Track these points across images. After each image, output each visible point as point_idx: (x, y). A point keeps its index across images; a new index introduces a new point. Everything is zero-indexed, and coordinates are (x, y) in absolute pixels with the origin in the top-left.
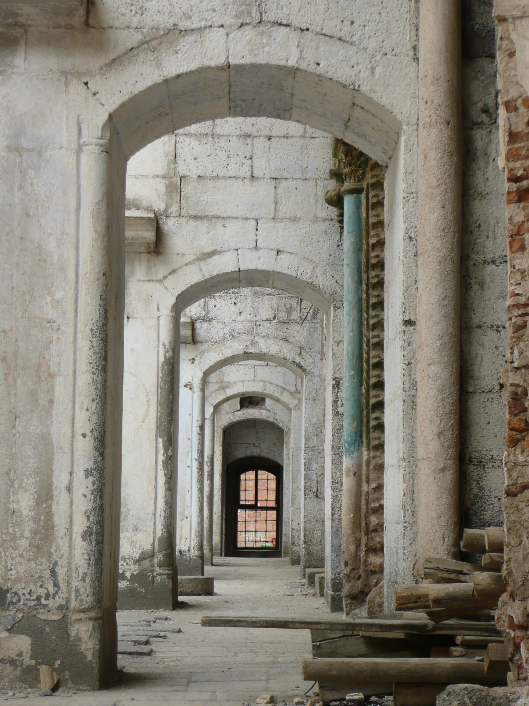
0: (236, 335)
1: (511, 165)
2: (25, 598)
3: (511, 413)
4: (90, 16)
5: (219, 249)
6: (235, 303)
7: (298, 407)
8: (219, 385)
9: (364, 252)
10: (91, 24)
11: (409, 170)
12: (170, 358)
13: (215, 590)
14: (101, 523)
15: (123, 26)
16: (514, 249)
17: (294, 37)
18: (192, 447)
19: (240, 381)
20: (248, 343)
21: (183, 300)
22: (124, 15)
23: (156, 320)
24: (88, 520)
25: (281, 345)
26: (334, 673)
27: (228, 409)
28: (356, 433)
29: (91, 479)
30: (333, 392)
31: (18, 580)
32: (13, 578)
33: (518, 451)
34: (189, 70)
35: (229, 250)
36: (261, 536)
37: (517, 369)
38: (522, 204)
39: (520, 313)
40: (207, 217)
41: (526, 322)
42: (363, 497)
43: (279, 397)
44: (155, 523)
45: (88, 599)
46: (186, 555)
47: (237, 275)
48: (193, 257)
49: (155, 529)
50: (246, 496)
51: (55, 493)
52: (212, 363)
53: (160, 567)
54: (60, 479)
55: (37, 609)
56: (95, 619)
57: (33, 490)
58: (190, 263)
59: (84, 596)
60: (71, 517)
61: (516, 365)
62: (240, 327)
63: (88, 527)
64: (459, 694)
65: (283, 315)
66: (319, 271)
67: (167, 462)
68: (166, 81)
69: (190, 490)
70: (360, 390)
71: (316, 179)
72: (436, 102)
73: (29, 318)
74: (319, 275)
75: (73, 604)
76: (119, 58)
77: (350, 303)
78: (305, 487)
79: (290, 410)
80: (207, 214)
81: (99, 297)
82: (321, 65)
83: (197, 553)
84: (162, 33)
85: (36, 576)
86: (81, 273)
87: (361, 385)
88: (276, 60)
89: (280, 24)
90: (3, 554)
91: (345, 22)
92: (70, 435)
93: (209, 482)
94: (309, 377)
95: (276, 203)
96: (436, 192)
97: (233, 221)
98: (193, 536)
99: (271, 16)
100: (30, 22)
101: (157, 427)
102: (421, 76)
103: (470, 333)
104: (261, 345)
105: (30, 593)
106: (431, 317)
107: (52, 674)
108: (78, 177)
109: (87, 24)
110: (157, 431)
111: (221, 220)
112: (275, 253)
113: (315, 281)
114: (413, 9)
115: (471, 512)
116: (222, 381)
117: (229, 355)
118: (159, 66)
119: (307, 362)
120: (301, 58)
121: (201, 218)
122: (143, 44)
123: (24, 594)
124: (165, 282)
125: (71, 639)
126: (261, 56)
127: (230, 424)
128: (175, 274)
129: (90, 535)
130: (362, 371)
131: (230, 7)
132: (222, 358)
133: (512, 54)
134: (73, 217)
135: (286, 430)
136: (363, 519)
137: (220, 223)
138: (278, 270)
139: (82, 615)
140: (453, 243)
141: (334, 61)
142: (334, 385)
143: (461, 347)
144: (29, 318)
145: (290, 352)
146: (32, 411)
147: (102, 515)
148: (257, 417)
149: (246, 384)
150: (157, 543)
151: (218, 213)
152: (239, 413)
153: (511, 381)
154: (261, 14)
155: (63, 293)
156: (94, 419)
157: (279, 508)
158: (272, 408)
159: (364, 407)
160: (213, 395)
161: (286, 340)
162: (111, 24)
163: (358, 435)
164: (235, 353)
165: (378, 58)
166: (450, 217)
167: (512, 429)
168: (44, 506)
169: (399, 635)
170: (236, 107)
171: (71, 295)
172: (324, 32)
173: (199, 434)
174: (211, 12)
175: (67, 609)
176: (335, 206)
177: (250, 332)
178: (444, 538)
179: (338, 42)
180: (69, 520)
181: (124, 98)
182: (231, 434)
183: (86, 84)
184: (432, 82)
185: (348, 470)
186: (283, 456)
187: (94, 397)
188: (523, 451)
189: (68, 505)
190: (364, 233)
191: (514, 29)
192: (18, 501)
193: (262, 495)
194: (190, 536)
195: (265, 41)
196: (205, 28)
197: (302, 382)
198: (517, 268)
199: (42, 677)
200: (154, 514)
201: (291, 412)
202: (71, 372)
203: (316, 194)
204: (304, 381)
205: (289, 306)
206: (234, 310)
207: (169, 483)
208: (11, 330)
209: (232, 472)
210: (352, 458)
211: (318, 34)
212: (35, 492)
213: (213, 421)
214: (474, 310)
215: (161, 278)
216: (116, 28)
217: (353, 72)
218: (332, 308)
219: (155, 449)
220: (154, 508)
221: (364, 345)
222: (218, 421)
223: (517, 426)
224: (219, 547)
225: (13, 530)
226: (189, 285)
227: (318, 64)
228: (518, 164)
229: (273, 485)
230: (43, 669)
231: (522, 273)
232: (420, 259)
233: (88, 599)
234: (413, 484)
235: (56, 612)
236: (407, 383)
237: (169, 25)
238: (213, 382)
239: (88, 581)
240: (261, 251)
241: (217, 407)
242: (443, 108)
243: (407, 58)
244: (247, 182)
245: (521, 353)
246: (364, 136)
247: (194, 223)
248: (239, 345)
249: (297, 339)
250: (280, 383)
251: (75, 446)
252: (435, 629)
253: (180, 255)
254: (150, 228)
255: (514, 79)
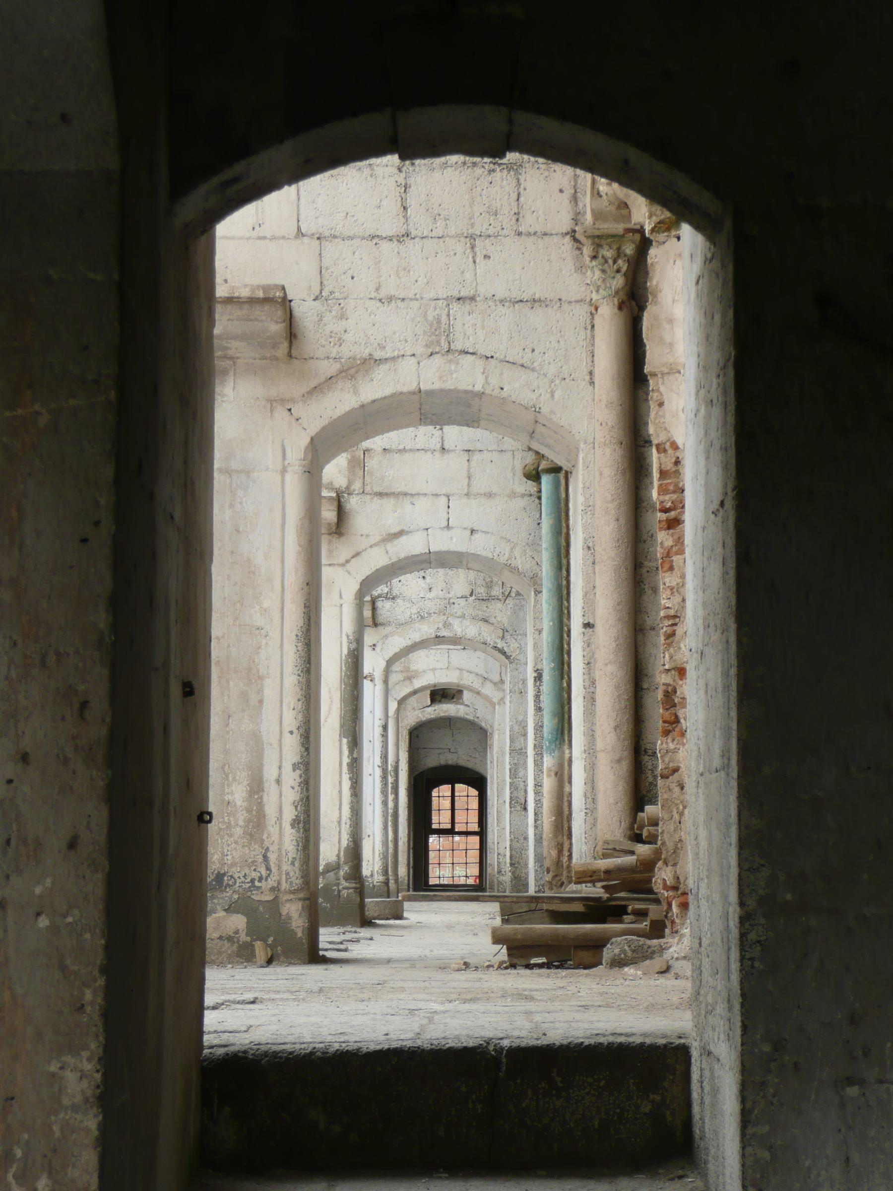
5: (407, 529)
6: (424, 577)
8: (405, 674)
9: (563, 535)
10: (293, 355)
11: (587, 485)
12: (354, 650)
13: (405, 915)
14: (307, 812)
16: (665, 569)
17: (480, 364)
18: (373, 751)
20: (440, 625)
21: (367, 584)
22: (323, 346)
26: (519, 937)
29: (298, 772)
30: (535, 685)
31: (234, 864)
32: (229, 862)
33: (669, 740)
35: (418, 530)
36: (459, 871)
37: (668, 670)
38: (671, 531)
40: (394, 493)
42: (566, 799)
44: (340, 832)
45: (297, 881)
47: (427, 557)
48: (378, 538)
50: (440, 818)
51: (266, 785)
52: (397, 650)
53: (346, 879)
54: (270, 773)
57: (245, 783)
58: (376, 545)
59: (293, 879)
61: (667, 667)
62: (430, 606)
66: (517, 553)
68: (363, 406)
70: (562, 684)
72: (610, 424)
73: (240, 625)
75: (284, 886)
77: (550, 590)
78: (511, 798)
79: (493, 705)
80: (393, 491)
85: (250, 860)
86: (286, 583)
87: (562, 678)
88: (462, 386)
89: (467, 353)
93: (393, 796)
96: (611, 506)
97: (422, 497)
98: (377, 859)
99: (458, 345)
101: (342, 726)
103: (644, 634)
104: (455, 627)
105: (245, 876)
108: (283, 496)
109: (290, 355)
112: (469, 532)
113: (513, 563)
114: (589, 337)
116: (407, 670)
118: (356, 392)
119: (511, 647)
120: (487, 382)
121: (387, 495)
123: (239, 877)
124: (348, 565)
125: (283, 917)
128: (359, 558)
129: (298, 824)
131: (421, 337)
132: (409, 643)
133: (661, 404)
134: (279, 533)
135: (490, 731)
136: (565, 822)
137: (407, 500)
138: (472, 552)
139: (292, 896)
140: (626, 553)
141: (517, 385)
143: (636, 647)
145: (491, 635)
146: (243, 711)
147: (308, 806)
149: (437, 673)
150: (342, 853)
152: (430, 709)
153: (663, 681)
155: (270, 602)
156: (300, 717)
157: (482, 833)
159: (566, 702)
160: (397, 687)
161: (485, 621)
164: (425, 637)
165: (557, 382)
167: (664, 722)
169: (578, 907)
170: (426, 419)
172: (507, 359)
173: (383, 736)
175: (279, 890)
177: (442, 612)
179: (520, 368)
181: (325, 422)
182: (418, 736)
183: (290, 410)
184: (606, 406)
185: (549, 770)
187: (299, 697)
188: (673, 740)
189: (278, 796)
190: (563, 514)
191: (663, 383)
192: (232, 793)
193: (460, 817)
195: (453, 368)
196: (398, 357)
199: (257, 951)
200: (339, 822)
201: (494, 708)
203: (513, 469)
206: (423, 585)
208: (223, 637)
209: (422, 785)
211: (501, 361)
212: (248, 785)
213: (397, 720)
215: (344, 562)
218: (533, 593)
219: (338, 750)
221: (565, 635)
224: (406, 882)
226: (374, 569)
227: (502, 389)
228: (667, 497)
229: (474, 804)
230: (258, 944)
232: (597, 567)
233: (297, 881)
236: (587, 680)
237: (365, 354)
240: (454, 531)
241: (401, 702)
244: (437, 454)
245: (671, 657)
246: (548, 446)
247: (379, 501)
249: (499, 619)
252: (609, 899)
254: (331, 508)
255: (663, 426)
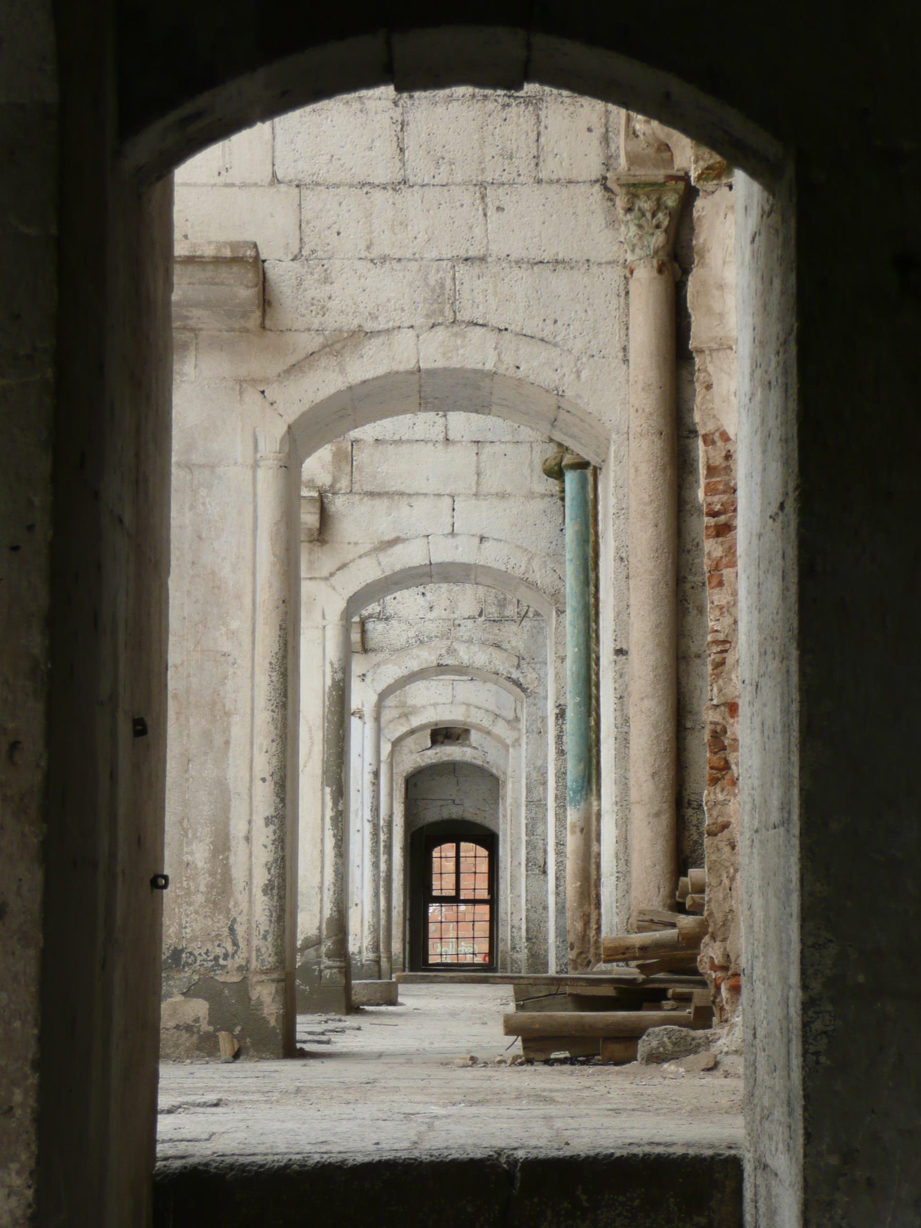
0: (426, 639)
1: (709, 499)
2: (202, 958)
3: (711, 752)
4: (267, 318)
5: (403, 536)
6: (423, 594)
7: (517, 741)
8: (400, 711)
9: (591, 544)
10: (267, 326)
11: (620, 483)
12: (339, 681)
14: (282, 876)
15: (302, 328)
17: (491, 338)
18: (362, 802)
19: (431, 705)
20: (443, 651)
21: (355, 602)
22: (304, 316)
23: (321, 631)
24: (269, 873)
25: (491, 654)
26: (537, 1026)
27: (413, 747)
28: (583, 778)
29: (272, 827)
30: (557, 724)
31: (194, 939)
32: (188, 936)
33: (718, 790)
34: (375, 376)
35: (416, 537)
36: (465, 947)
37: (717, 706)
38: (721, 539)
39: (719, 649)
40: (387, 493)
41: (724, 659)
42: (593, 860)
43: (490, 728)
44: (321, 900)
45: (270, 959)
46: (355, 960)
47: (428, 569)
48: (368, 547)
49: (321, 908)
50: (442, 884)
51: (233, 843)
52: (391, 681)
54: (238, 828)
55: (215, 970)
56: (278, 981)
57: (208, 840)
58: (366, 554)
59: (265, 956)
60: (250, 870)
61: (715, 702)
62: (431, 628)
63: (269, 880)
64: (658, 1035)
65: (493, 610)
66: (536, 564)
67: (337, 818)
68: (350, 388)
69: (360, 864)
70: (588, 722)
71: (531, 443)
72: (647, 410)
73: (202, 651)
74: (536, 570)
75: (254, 964)
76: (298, 363)
77: (575, 610)
78: (527, 859)
79: (506, 747)
80: (387, 489)
81: (278, 627)
82: (521, 369)
83: (371, 956)
84: (346, 335)
85: (214, 934)
86: (258, 601)
87: (590, 716)
88: (470, 364)
89: (476, 324)
90: (177, 910)
91: (547, 321)
92: (248, 779)
94: (531, 700)
95: (478, 474)
97: (421, 498)
98: (366, 932)
100: (200, 326)
101: (324, 773)
102: (631, 378)
103: (688, 664)
104: (461, 653)
105: (207, 953)
106: (643, 646)
107: (232, 1041)
108: (255, 495)
109: (263, 327)
110: (323, 778)
111: (405, 497)
112: (477, 540)
113: (531, 576)
115: (691, 860)
116: (403, 705)
117: (415, 670)
118: (342, 371)
119: (528, 677)
120: (500, 360)
122: (324, 347)
123: (200, 954)
124: (333, 580)
125: (253, 1003)
126: (455, 359)
127: (415, 769)
129: (272, 889)
130: (590, 697)
131: (421, 305)
132: (406, 672)
133: (709, 387)
134: (249, 539)
135: (502, 778)
136: (593, 888)
137: (404, 502)
138: (482, 563)
139: (264, 977)
140: (667, 565)
142: (557, 714)
144: (202, 651)
145: (503, 663)
146: (206, 754)
148: (458, 759)
149: (439, 708)
150: (324, 925)
151: (402, 488)
152: (429, 752)
153: (711, 719)
154: (454, 312)
156: (274, 761)
157: (493, 902)
158: (480, 745)
159: (593, 744)
160: (391, 726)
161: (497, 646)
162: (289, 327)
163: (586, 780)
164: (424, 666)
165: (584, 360)
166: (663, 537)
167: (712, 768)
168: (221, 857)
170: (426, 403)
171: (248, 625)
172: (524, 332)
173: (374, 784)
174: (399, 312)
175: (247, 970)
176: (556, 479)
177: (445, 635)
178: (659, 888)
179: (540, 343)
180: (247, 873)
181: (306, 407)
182: (416, 785)
183: (263, 392)
184: (643, 389)
185: (574, 826)
186: (498, 818)
187: (274, 737)
188: (723, 790)
191: (711, 362)
192: (192, 853)
194: (362, 931)
195: (459, 342)
196: (393, 329)
197: (522, 706)
198: (716, 603)
200: (321, 888)
201: (508, 751)
202: (248, 711)
203: (531, 462)
204: (525, 706)
205: (502, 597)
206: (423, 603)
207: (340, 847)
208: (182, 664)
209: (421, 843)
210: (578, 810)
211: (517, 334)
212: (211, 843)
214: (692, 638)
216: (295, 331)
217: (556, 377)
218: (554, 613)
220: (319, 880)
222: (398, 765)
223: (716, 765)
224: (401, 960)
225: (188, 884)
226: (364, 584)
227: (518, 368)
228: (716, 499)
229: (483, 866)
230: (223, 1036)
231: (721, 609)
232: (632, 582)
233: (270, 959)
234: (626, 831)
235: (235, 973)
238: (390, 707)
239: (270, 939)
241: (396, 744)
242: (655, 418)
243: (616, 361)
244: (440, 446)
245: (720, 690)
246: (573, 437)
247: (370, 502)
248: (430, 654)
249: (514, 644)
250: (492, 707)
251: (253, 792)
252: (645, 982)
253: (352, 545)
254: (313, 510)
